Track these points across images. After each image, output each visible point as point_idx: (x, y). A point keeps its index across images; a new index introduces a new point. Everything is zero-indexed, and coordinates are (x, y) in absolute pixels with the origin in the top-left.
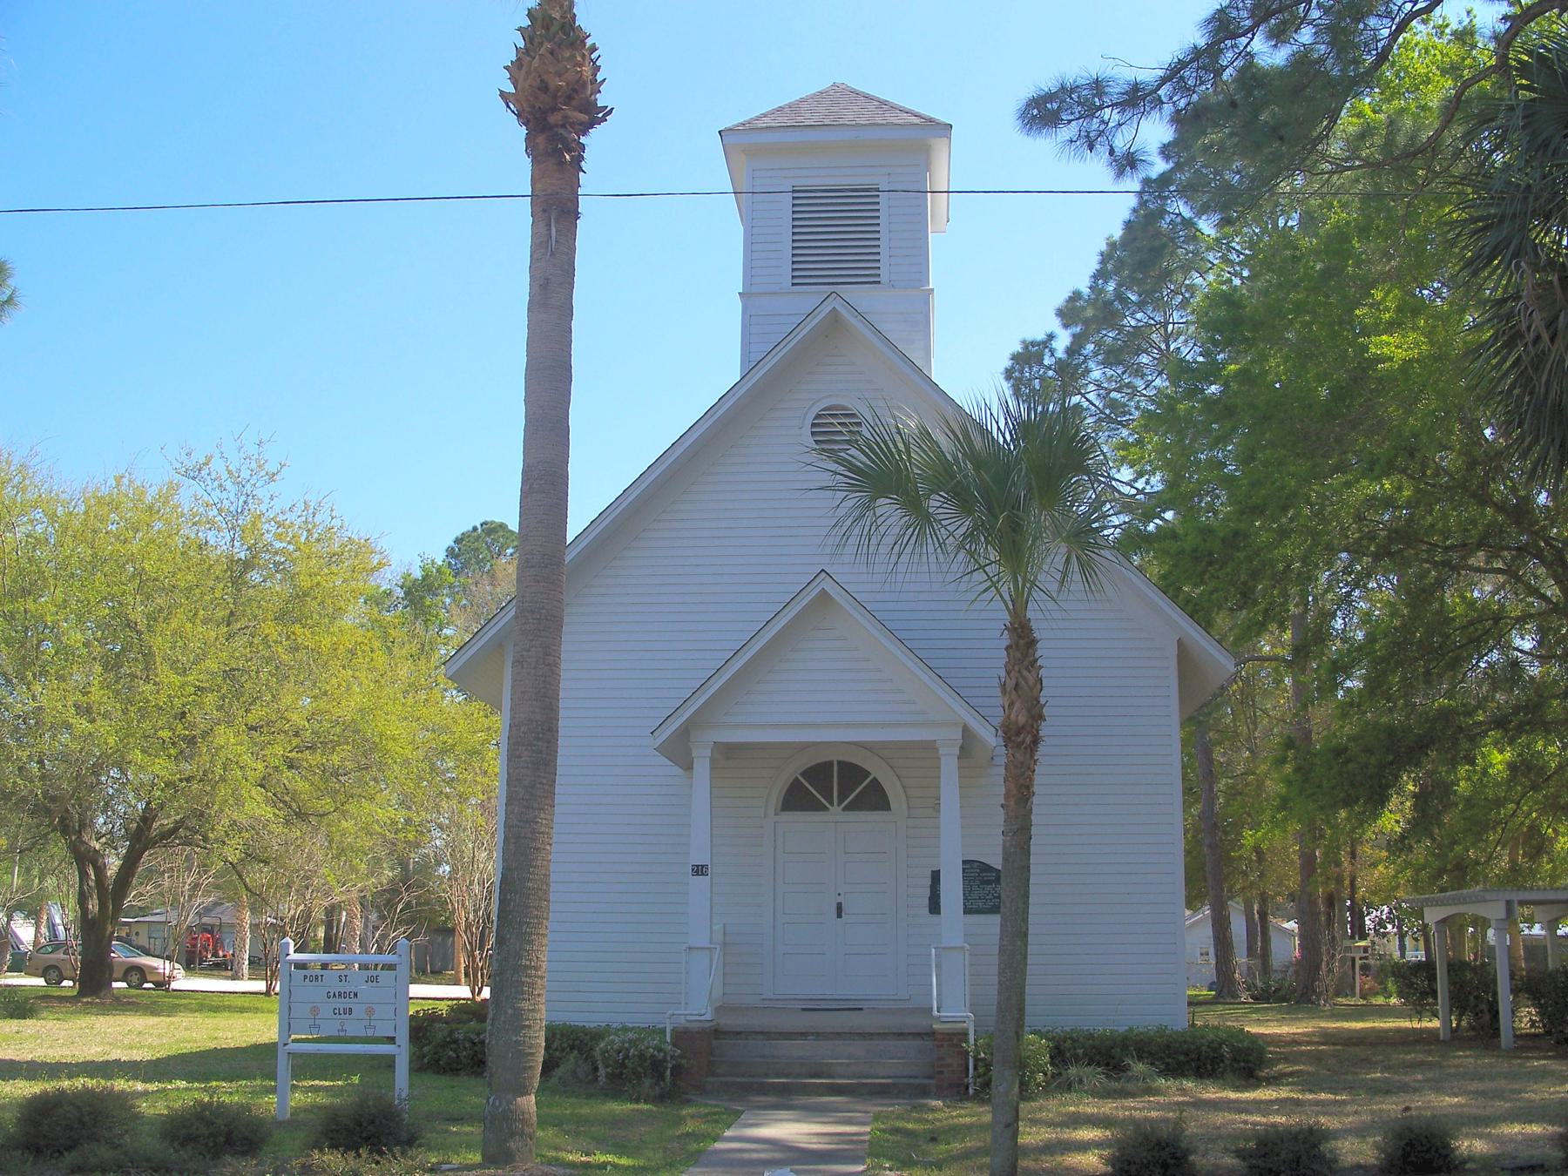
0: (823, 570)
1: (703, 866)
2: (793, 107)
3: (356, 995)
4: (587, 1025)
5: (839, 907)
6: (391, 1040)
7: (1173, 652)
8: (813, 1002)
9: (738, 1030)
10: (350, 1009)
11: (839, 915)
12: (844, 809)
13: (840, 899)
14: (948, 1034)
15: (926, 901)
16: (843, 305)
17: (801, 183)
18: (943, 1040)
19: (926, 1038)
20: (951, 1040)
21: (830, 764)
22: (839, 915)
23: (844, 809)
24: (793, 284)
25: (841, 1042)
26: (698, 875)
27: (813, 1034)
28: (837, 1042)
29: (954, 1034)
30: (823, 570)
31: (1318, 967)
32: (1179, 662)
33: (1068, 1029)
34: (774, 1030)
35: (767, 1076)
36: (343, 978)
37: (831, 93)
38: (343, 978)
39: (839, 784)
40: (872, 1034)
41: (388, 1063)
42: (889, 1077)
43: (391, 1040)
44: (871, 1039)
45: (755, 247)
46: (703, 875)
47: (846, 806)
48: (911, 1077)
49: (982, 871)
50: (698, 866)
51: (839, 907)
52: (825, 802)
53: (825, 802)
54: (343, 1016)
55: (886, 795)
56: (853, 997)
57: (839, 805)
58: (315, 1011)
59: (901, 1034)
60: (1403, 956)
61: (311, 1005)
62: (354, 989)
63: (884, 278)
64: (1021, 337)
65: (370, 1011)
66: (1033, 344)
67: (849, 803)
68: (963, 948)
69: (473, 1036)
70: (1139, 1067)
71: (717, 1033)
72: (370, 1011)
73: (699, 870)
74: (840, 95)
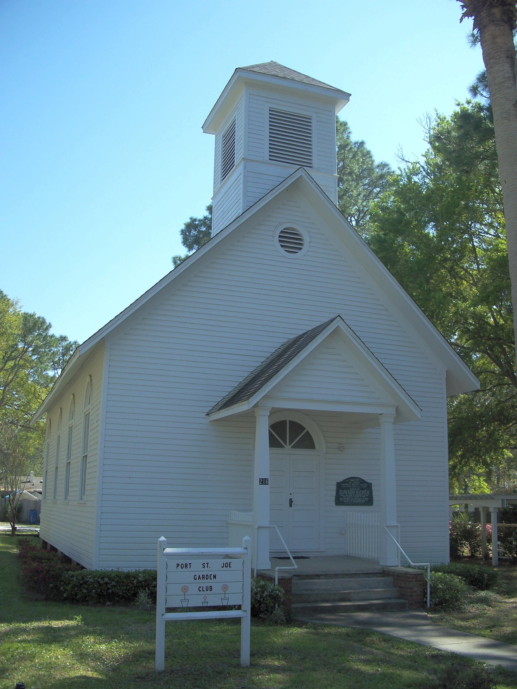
0: (339, 315)
1: (265, 479)
3: (215, 577)
4: (107, 569)
5: (291, 501)
6: (239, 607)
7: (444, 376)
10: (211, 587)
11: (291, 506)
12: (292, 447)
13: (291, 497)
14: (415, 575)
18: (413, 578)
19: (379, 575)
20: (416, 577)
21: (285, 422)
22: (291, 506)
23: (292, 447)
24: (270, 159)
26: (263, 484)
27: (323, 575)
30: (339, 315)
32: (447, 381)
34: (312, 574)
35: (317, 601)
36: (206, 565)
37: (271, 63)
38: (206, 565)
39: (289, 431)
40: (352, 574)
41: (237, 621)
42: (382, 599)
43: (239, 607)
44: (352, 577)
46: (266, 484)
48: (388, 598)
50: (263, 479)
51: (291, 501)
52: (293, 444)
53: (293, 444)
54: (206, 592)
55: (313, 442)
57: (290, 444)
58: (185, 589)
59: (367, 574)
60: (63, 496)
61: (182, 585)
62: (213, 573)
64: (190, 216)
65: (225, 588)
66: (195, 220)
67: (294, 445)
68: (397, 526)
72: (225, 588)
73: (263, 482)
74: (273, 64)
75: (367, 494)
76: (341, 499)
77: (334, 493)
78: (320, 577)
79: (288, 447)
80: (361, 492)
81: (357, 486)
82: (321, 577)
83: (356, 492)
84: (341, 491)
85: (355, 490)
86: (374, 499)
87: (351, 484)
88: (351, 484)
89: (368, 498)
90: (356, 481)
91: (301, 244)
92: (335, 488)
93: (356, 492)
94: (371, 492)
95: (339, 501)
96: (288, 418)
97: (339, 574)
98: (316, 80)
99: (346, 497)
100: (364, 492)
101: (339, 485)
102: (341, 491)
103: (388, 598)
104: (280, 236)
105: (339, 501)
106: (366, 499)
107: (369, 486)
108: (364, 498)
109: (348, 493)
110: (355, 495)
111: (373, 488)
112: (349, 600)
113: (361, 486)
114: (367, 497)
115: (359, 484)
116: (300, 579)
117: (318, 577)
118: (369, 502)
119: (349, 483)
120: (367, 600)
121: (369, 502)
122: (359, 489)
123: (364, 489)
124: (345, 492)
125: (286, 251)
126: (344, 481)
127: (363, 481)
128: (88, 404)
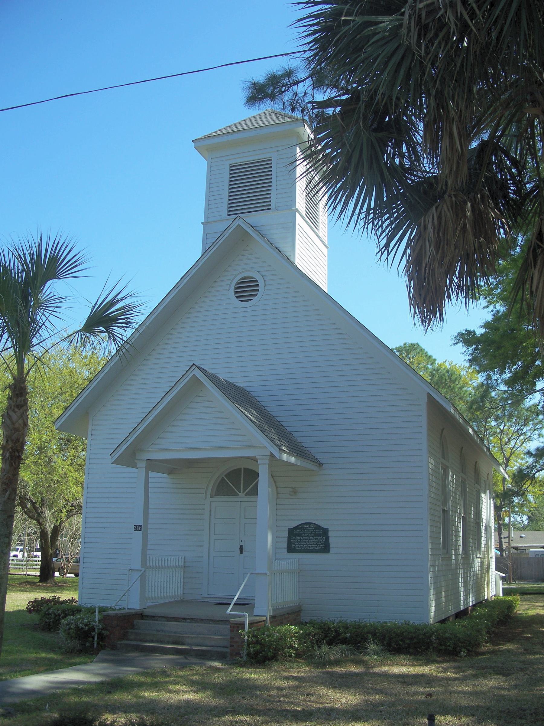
0: (194, 364)
2: (236, 125)
5: (241, 548)
8: (227, 600)
9: (152, 615)
11: (241, 553)
12: (246, 495)
13: (242, 544)
14: (236, 624)
15: (285, 545)
16: (243, 222)
17: (233, 162)
22: (241, 553)
23: (246, 495)
25: (196, 624)
27: (189, 619)
28: (193, 624)
29: (240, 624)
30: (194, 364)
31: (176, 601)
33: (357, 620)
34: (169, 616)
39: (244, 479)
45: (211, 198)
47: (247, 493)
48: (224, 647)
49: (316, 528)
51: (241, 548)
56: (246, 598)
63: (272, 207)
69: (55, 611)
70: (372, 647)
71: (141, 616)
75: (322, 541)
76: (293, 546)
77: (286, 540)
78: (186, 620)
79: (242, 495)
80: (316, 539)
81: (311, 532)
82: (187, 621)
83: (309, 538)
84: (293, 538)
85: (309, 537)
86: (331, 546)
87: (304, 530)
88: (304, 530)
89: (324, 545)
90: (310, 527)
91: (236, 293)
92: (287, 534)
93: (309, 538)
94: (327, 538)
95: (291, 549)
96: (243, 465)
97: (205, 619)
98: (239, 123)
99: (299, 544)
100: (318, 538)
101: (292, 532)
102: (293, 538)
103: (224, 647)
104: (258, 285)
105: (291, 549)
106: (321, 545)
107: (325, 532)
108: (320, 545)
109: (301, 540)
110: (308, 541)
111: (330, 534)
112: (183, 644)
113: (316, 532)
114: (322, 544)
115: (313, 530)
116: (167, 621)
117: (185, 621)
118: (326, 548)
119: (302, 529)
120: (201, 646)
121: (326, 548)
122: (313, 535)
123: (319, 535)
124: (298, 538)
125: (240, 301)
126: (297, 528)
127: (318, 527)
128: (256, 462)
